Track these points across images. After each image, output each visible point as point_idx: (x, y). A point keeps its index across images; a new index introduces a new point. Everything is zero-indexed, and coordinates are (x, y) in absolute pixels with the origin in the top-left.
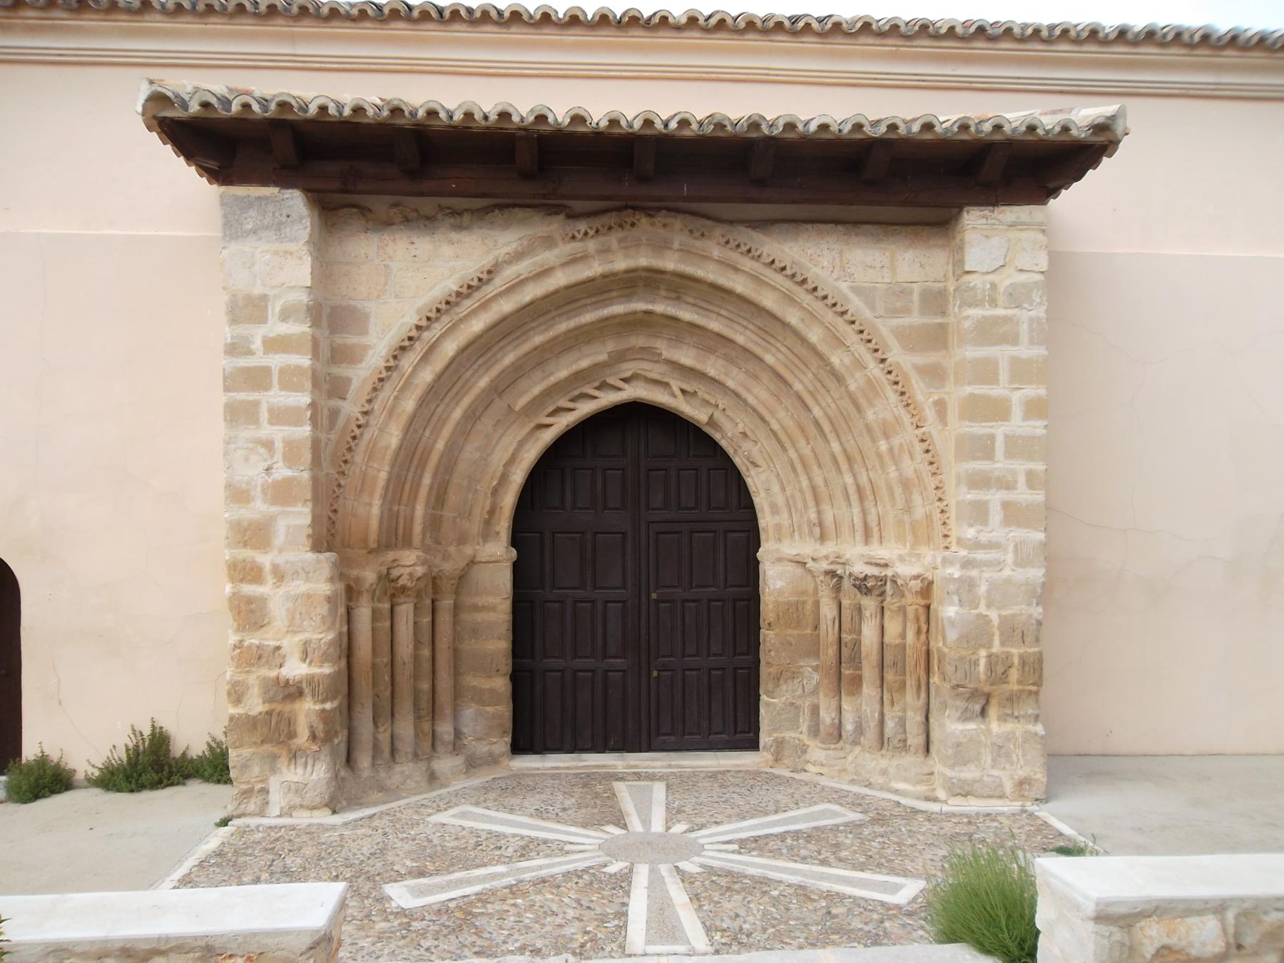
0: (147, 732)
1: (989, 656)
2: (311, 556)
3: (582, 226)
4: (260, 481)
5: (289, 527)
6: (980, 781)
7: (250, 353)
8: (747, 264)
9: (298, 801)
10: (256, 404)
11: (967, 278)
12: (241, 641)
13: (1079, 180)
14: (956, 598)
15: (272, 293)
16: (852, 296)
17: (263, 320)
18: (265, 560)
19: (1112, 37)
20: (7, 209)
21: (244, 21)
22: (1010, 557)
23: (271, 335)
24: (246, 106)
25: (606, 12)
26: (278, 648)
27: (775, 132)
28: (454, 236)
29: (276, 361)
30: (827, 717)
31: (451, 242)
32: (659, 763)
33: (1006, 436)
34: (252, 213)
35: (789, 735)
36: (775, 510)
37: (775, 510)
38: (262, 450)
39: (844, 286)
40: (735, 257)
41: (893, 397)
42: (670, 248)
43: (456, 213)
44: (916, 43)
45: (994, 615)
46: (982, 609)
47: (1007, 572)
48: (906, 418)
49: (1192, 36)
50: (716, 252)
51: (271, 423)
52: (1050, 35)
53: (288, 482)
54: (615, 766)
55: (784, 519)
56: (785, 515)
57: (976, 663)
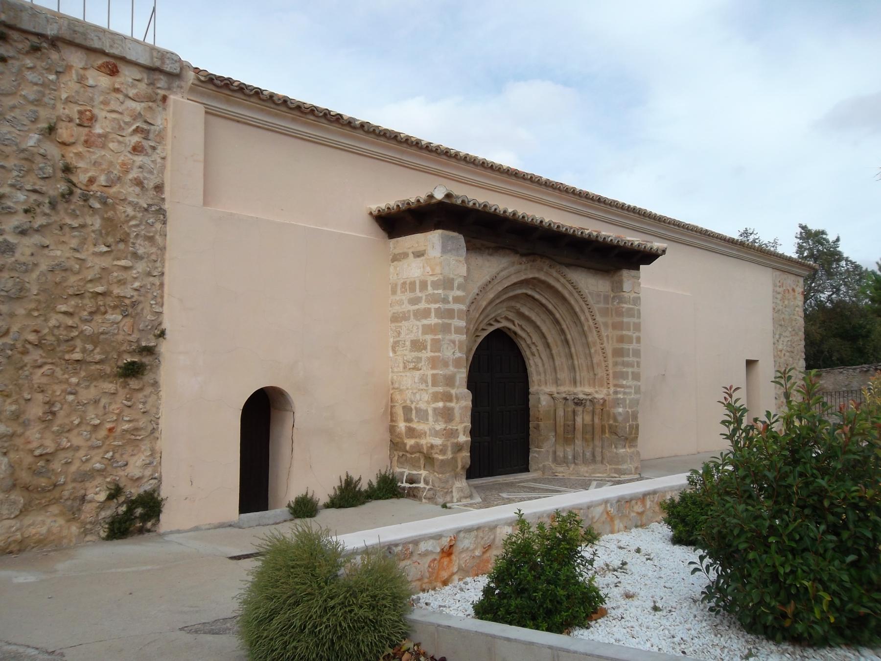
0: (344, 478)
1: (629, 426)
2: (466, 390)
3: (524, 259)
4: (452, 358)
5: (460, 378)
6: (627, 469)
7: (449, 302)
8: (562, 280)
9: (462, 495)
10: (450, 324)
11: (624, 293)
12: (446, 427)
13: (649, 264)
14: (621, 406)
15: (455, 277)
16: (589, 296)
17: (452, 289)
18: (453, 392)
19: (345, 123)
20: (282, 210)
21: (337, 125)
22: (633, 391)
23: (455, 295)
24: (474, 204)
25: (484, 161)
26: (457, 430)
27: (480, 208)
28: (489, 258)
29: (456, 307)
30: (560, 454)
31: (488, 261)
32: (512, 478)
33: (633, 349)
34: (450, 243)
35: (546, 463)
36: (539, 374)
37: (539, 374)
38: (452, 345)
39: (587, 291)
40: (559, 276)
41: (595, 333)
42: (542, 271)
43: (488, 248)
44: (252, 100)
45: (630, 411)
46: (627, 409)
47: (633, 396)
48: (598, 341)
49: (479, 162)
50: (555, 274)
51: (455, 334)
52: (368, 130)
53: (460, 358)
54: (499, 481)
55: (542, 377)
56: (543, 375)
57: (626, 428)
